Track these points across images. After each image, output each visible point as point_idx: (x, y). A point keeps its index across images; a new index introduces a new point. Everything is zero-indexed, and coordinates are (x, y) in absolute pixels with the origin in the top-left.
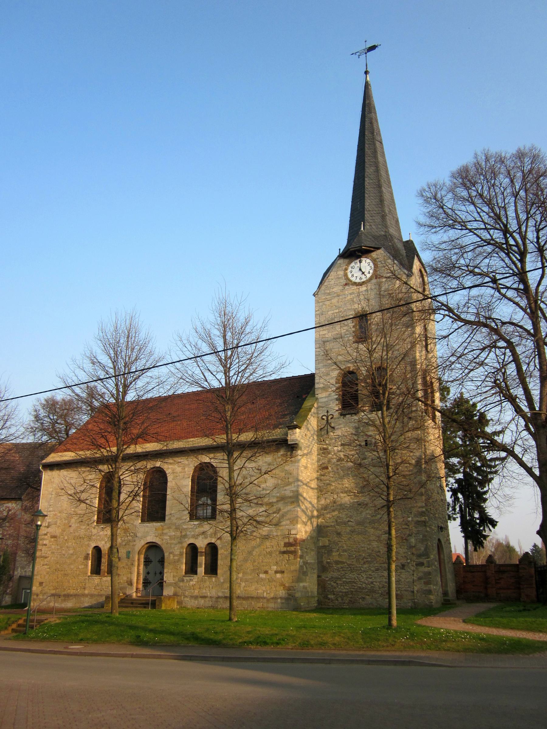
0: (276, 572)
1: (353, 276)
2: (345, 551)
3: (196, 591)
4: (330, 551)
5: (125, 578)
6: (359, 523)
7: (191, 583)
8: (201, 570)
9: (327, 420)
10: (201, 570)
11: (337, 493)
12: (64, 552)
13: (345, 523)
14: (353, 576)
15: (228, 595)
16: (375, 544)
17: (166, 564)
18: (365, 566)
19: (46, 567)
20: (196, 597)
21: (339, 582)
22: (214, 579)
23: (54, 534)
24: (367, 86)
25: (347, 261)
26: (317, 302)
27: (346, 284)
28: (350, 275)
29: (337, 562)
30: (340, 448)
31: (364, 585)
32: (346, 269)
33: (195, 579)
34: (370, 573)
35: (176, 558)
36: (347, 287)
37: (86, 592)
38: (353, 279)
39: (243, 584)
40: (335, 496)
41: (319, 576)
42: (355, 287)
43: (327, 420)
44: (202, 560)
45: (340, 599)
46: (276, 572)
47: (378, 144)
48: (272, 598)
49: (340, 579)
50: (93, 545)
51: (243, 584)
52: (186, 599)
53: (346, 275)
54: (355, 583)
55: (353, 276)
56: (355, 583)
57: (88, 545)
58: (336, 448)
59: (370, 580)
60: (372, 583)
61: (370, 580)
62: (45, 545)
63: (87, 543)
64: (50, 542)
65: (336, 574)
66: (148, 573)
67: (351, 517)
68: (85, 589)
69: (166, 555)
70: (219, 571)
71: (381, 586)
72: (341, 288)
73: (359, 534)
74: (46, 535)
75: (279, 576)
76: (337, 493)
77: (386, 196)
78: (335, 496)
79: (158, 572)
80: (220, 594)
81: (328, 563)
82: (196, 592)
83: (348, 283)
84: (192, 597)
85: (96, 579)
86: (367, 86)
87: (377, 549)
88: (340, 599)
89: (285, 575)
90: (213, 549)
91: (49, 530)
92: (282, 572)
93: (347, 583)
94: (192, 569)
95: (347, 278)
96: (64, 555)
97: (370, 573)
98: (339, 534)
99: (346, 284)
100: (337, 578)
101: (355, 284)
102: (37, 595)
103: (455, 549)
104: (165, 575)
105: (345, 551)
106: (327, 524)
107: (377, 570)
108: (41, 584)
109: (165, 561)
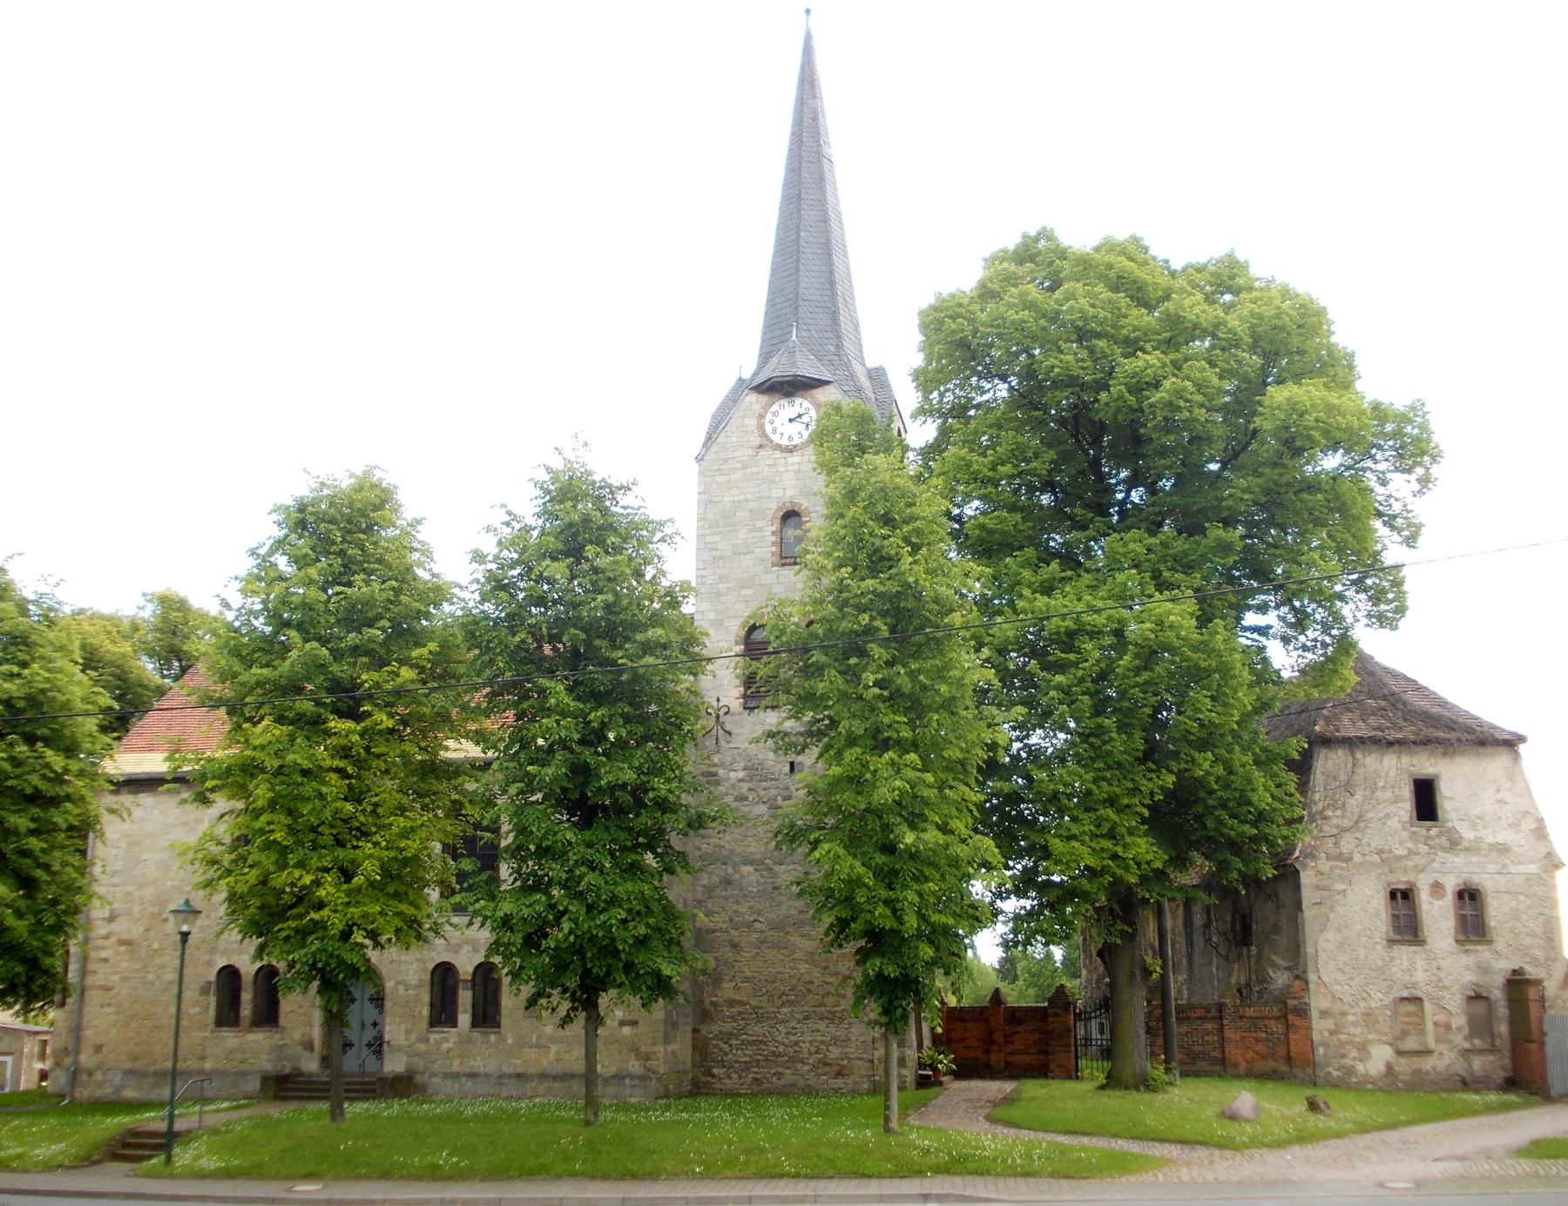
0: (622, 1023)
1: (774, 430)
2: (746, 980)
3: (456, 1062)
4: (717, 981)
5: (297, 1036)
6: (775, 926)
7: (445, 1045)
8: (464, 1019)
9: (718, 717)
10: (464, 1019)
11: (735, 866)
12: (150, 977)
13: (749, 925)
14: (758, 1029)
15: (580, 1067)
16: (803, 967)
17: (388, 1005)
18: (784, 1010)
19: (108, 1010)
20: (455, 1076)
21: (734, 1042)
22: (493, 1038)
23: (125, 936)
24: (808, 39)
25: (764, 399)
26: (701, 474)
27: (761, 446)
28: (768, 429)
29: (732, 1003)
30: (741, 774)
31: (781, 1049)
32: (762, 416)
33: (448, 1039)
34: (793, 1024)
35: (411, 992)
36: (762, 453)
37: (208, 1066)
38: (776, 438)
39: (554, 1048)
40: (730, 870)
41: (695, 1031)
42: (778, 454)
43: (718, 717)
44: (465, 997)
45: (735, 1076)
46: (622, 1023)
47: (826, 163)
48: (615, 1076)
49: (737, 1037)
50: (221, 962)
51: (554, 1048)
52: (434, 1080)
53: (761, 427)
54: (764, 1043)
55: (774, 430)
56: (764, 1043)
57: (210, 963)
58: (733, 775)
59: (793, 1038)
60: (796, 1043)
61: (793, 1038)
62: (106, 960)
63: (207, 958)
64: (117, 954)
65: (728, 1027)
66: (375, 1024)
67: (759, 913)
68: (203, 1058)
69: (389, 985)
70: (504, 1021)
71: (813, 1050)
72: (751, 452)
73: (774, 946)
74: (107, 937)
75: (626, 1030)
76: (735, 866)
77: (835, 236)
78: (730, 870)
79: (368, 1023)
80: (506, 1069)
81: (713, 1004)
82: (456, 1065)
83: (765, 443)
84: (446, 1076)
85: (231, 1038)
86: (808, 39)
87: (807, 978)
88: (735, 1076)
89: (640, 1029)
90: (485, 972)
91: (113, 927)
92: (634, 1023)
93: (750, 1043)
94: (443, 1013)
95: (764, 434)
96: (152, 984)
97: (793, 1024)
98: (735, 946)
99: (761, 446)
100: (731, 1034)
101: (779, 447)
102: (90, 1074)
103: (959, 1164)
104: (387, 1029)
105: (746, 980)
106: (712, 925)
107: (807, 1018)
108: (98, 1048)
109: (388, 998)
